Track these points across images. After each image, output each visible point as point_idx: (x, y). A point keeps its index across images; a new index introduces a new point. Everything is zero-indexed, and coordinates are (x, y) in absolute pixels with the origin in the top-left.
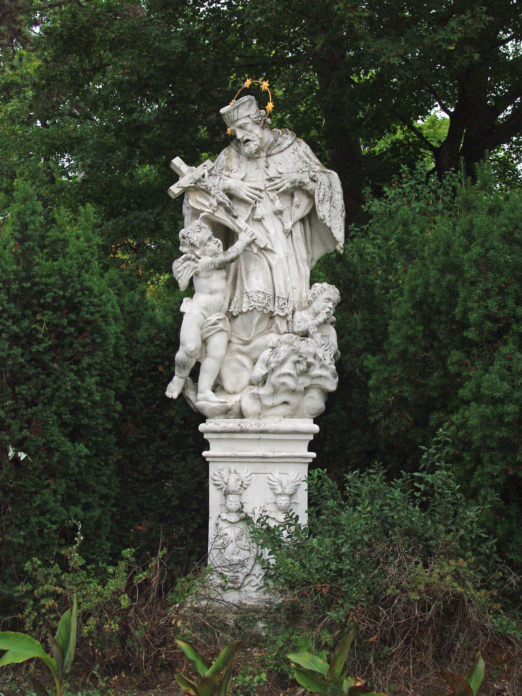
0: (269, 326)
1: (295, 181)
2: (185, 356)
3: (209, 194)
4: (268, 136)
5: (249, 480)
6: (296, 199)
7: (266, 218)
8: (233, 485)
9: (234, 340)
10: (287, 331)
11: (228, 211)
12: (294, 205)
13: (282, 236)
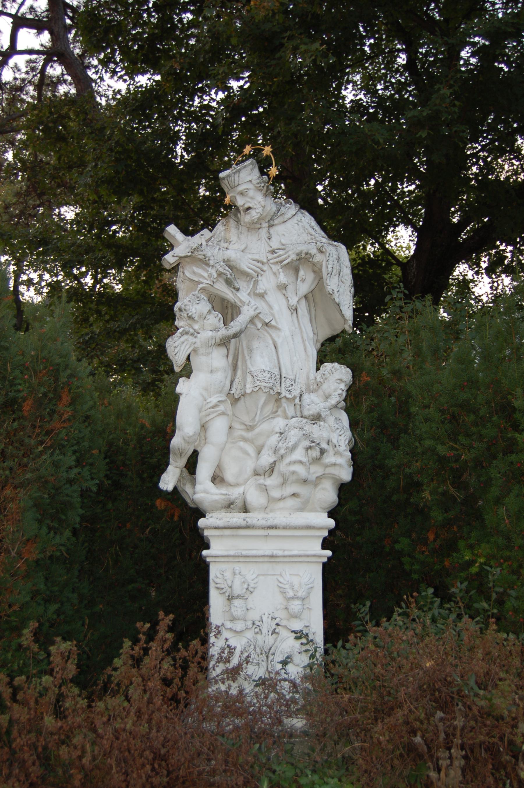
0: (274, 410)
1: (301, 252)
2: (183, 442)
3: (208, 265)
4: (270, 205)
5: (256, 583)
6: (301, 273)
7: (269, 293)
8: (238, 589)
9: (236, 425)
10: (294, 415)
11: (229, 282)
12: (299, 279)
13: (286, 312)
